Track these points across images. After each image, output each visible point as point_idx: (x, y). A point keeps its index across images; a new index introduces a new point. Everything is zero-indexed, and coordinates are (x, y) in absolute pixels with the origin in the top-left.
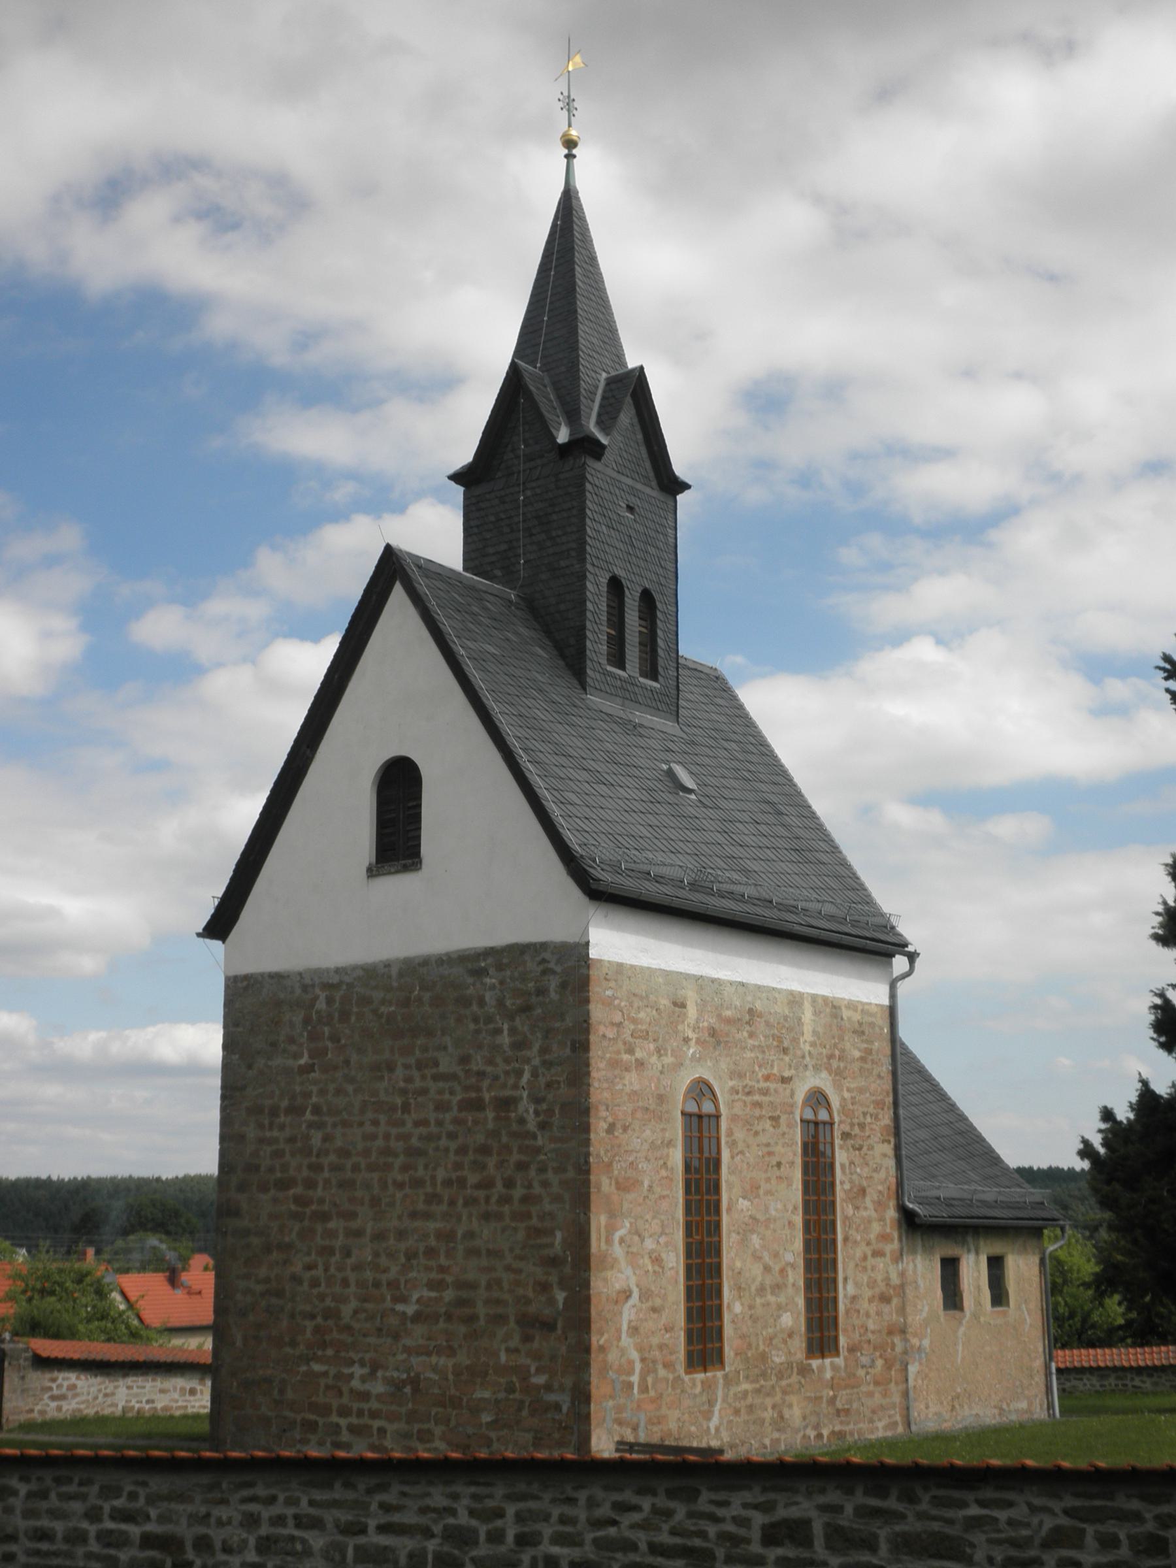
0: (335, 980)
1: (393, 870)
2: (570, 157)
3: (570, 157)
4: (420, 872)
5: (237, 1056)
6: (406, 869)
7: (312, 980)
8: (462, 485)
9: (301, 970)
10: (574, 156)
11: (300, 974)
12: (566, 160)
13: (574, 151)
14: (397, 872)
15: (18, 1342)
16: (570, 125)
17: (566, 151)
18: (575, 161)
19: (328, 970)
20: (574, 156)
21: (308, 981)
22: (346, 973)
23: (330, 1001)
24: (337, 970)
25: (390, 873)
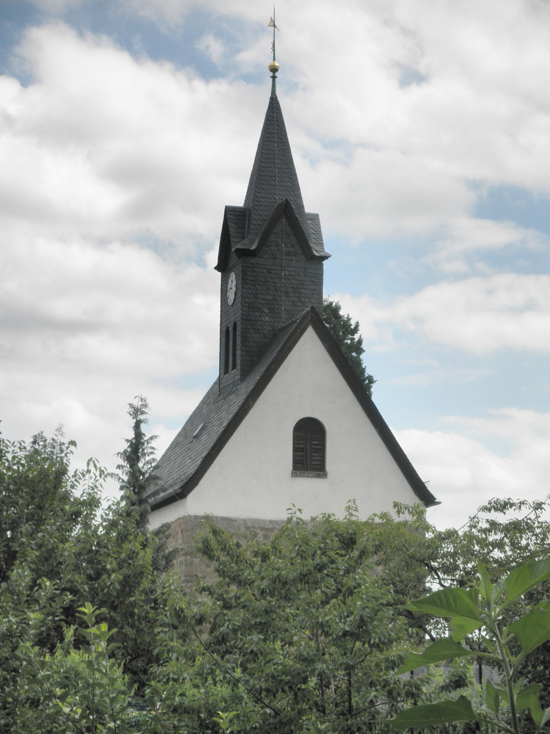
0: (270, 526)
1: (310, 475)
2: (274, 77)
3: (274, 77)
4: (326, 479)
5: (198, 560)
6: (319, 476)
7: (253, 524)
8: (245, 204)
9: (245, 518)
10: (276, 77)
11: (244, 520)
12: (271, 79)
13: (277, 74)
14: (313, 477)
15: (57, 657)
16: (274, 59)
17: (271, 74)
18: (276, 79)
19: (264, 521)
20: (276, 77)
21: (250, 524)
22: (277, 524)
23: (266, 537)
24: (271, 522)
25: (308, 477)
